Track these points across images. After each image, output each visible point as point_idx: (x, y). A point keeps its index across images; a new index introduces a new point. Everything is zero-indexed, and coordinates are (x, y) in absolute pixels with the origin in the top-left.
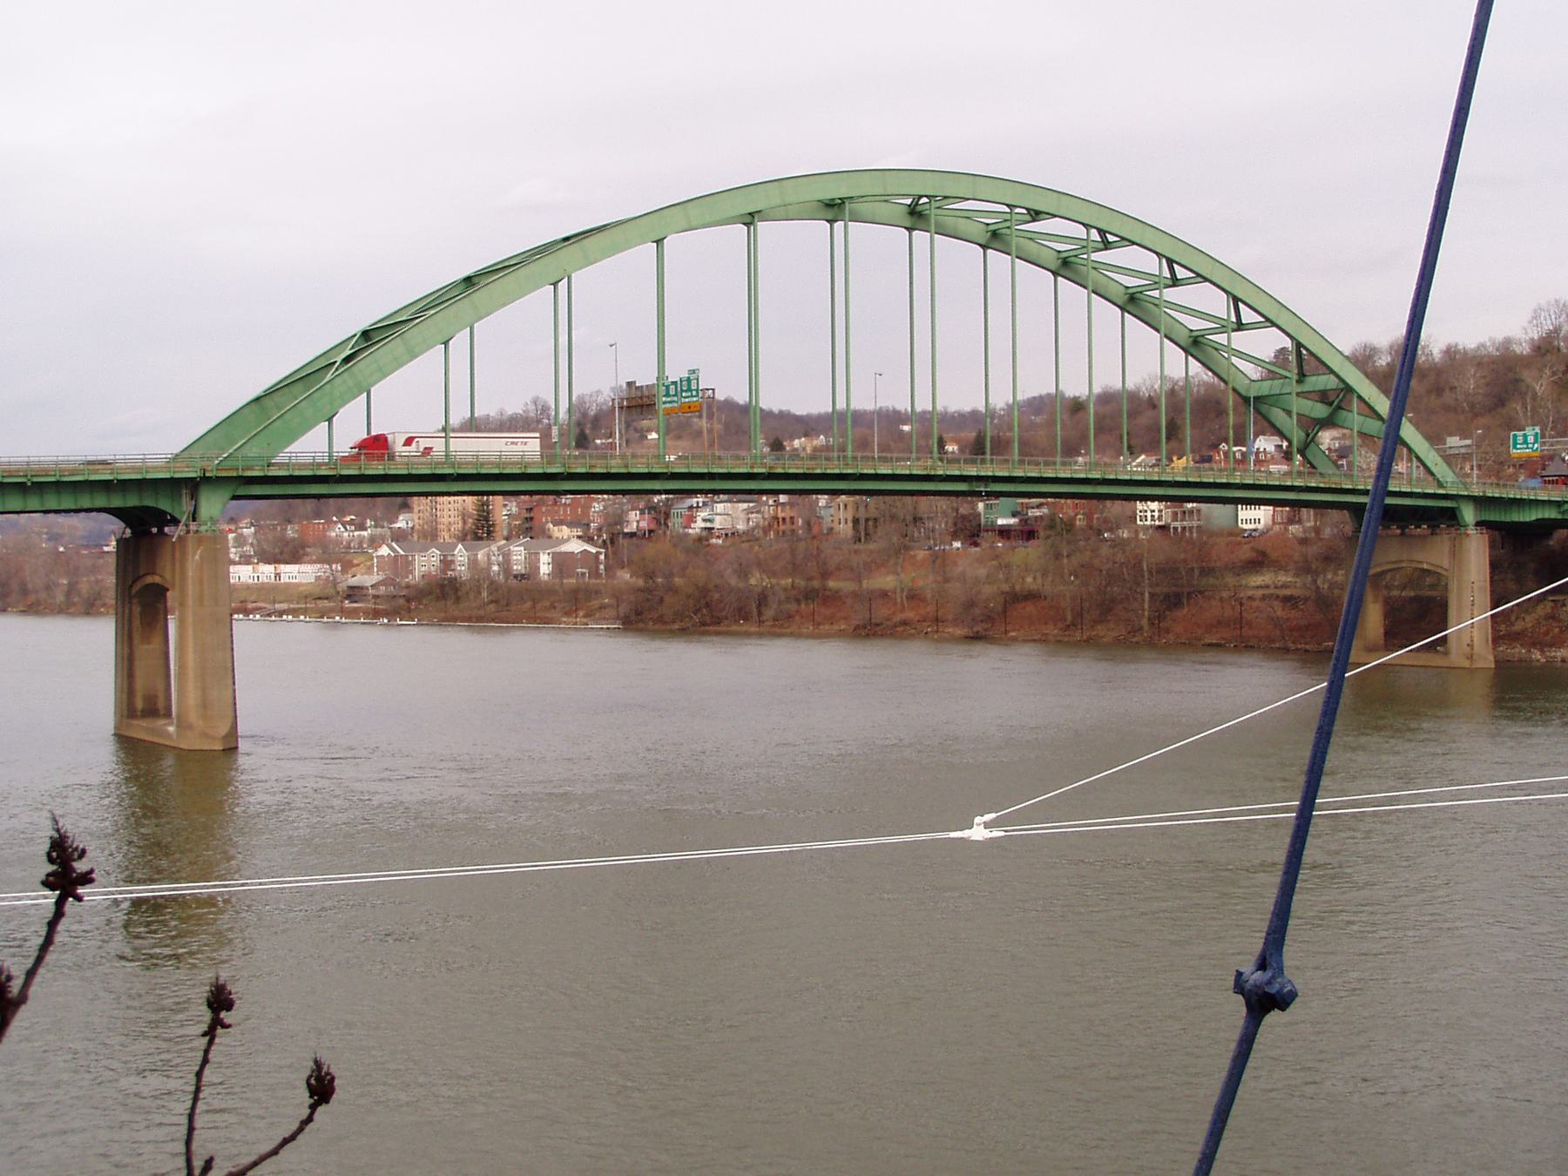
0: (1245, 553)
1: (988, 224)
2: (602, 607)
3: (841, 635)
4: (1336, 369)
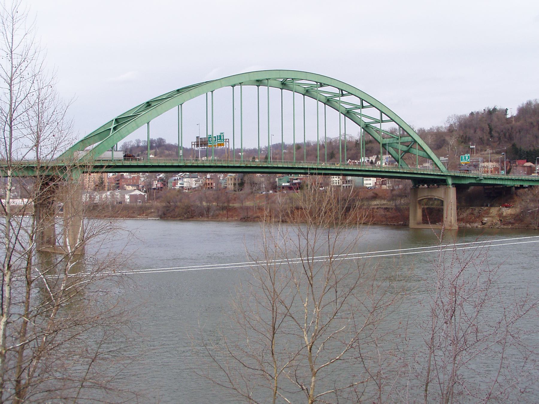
0: (370, 194)
1: (305, 88)
2: (151, 213)
3: (236, 220)
4: (412, 135)
